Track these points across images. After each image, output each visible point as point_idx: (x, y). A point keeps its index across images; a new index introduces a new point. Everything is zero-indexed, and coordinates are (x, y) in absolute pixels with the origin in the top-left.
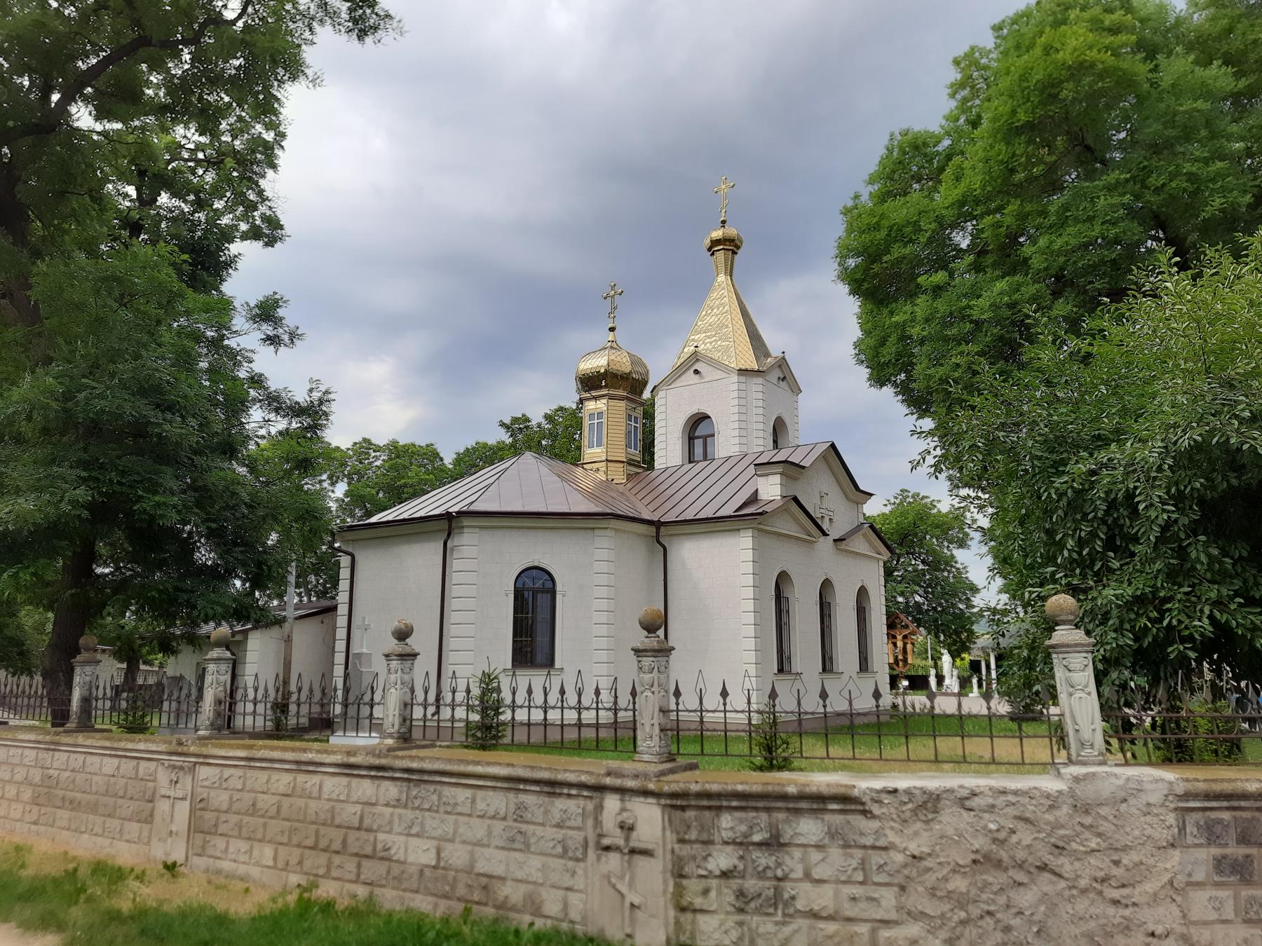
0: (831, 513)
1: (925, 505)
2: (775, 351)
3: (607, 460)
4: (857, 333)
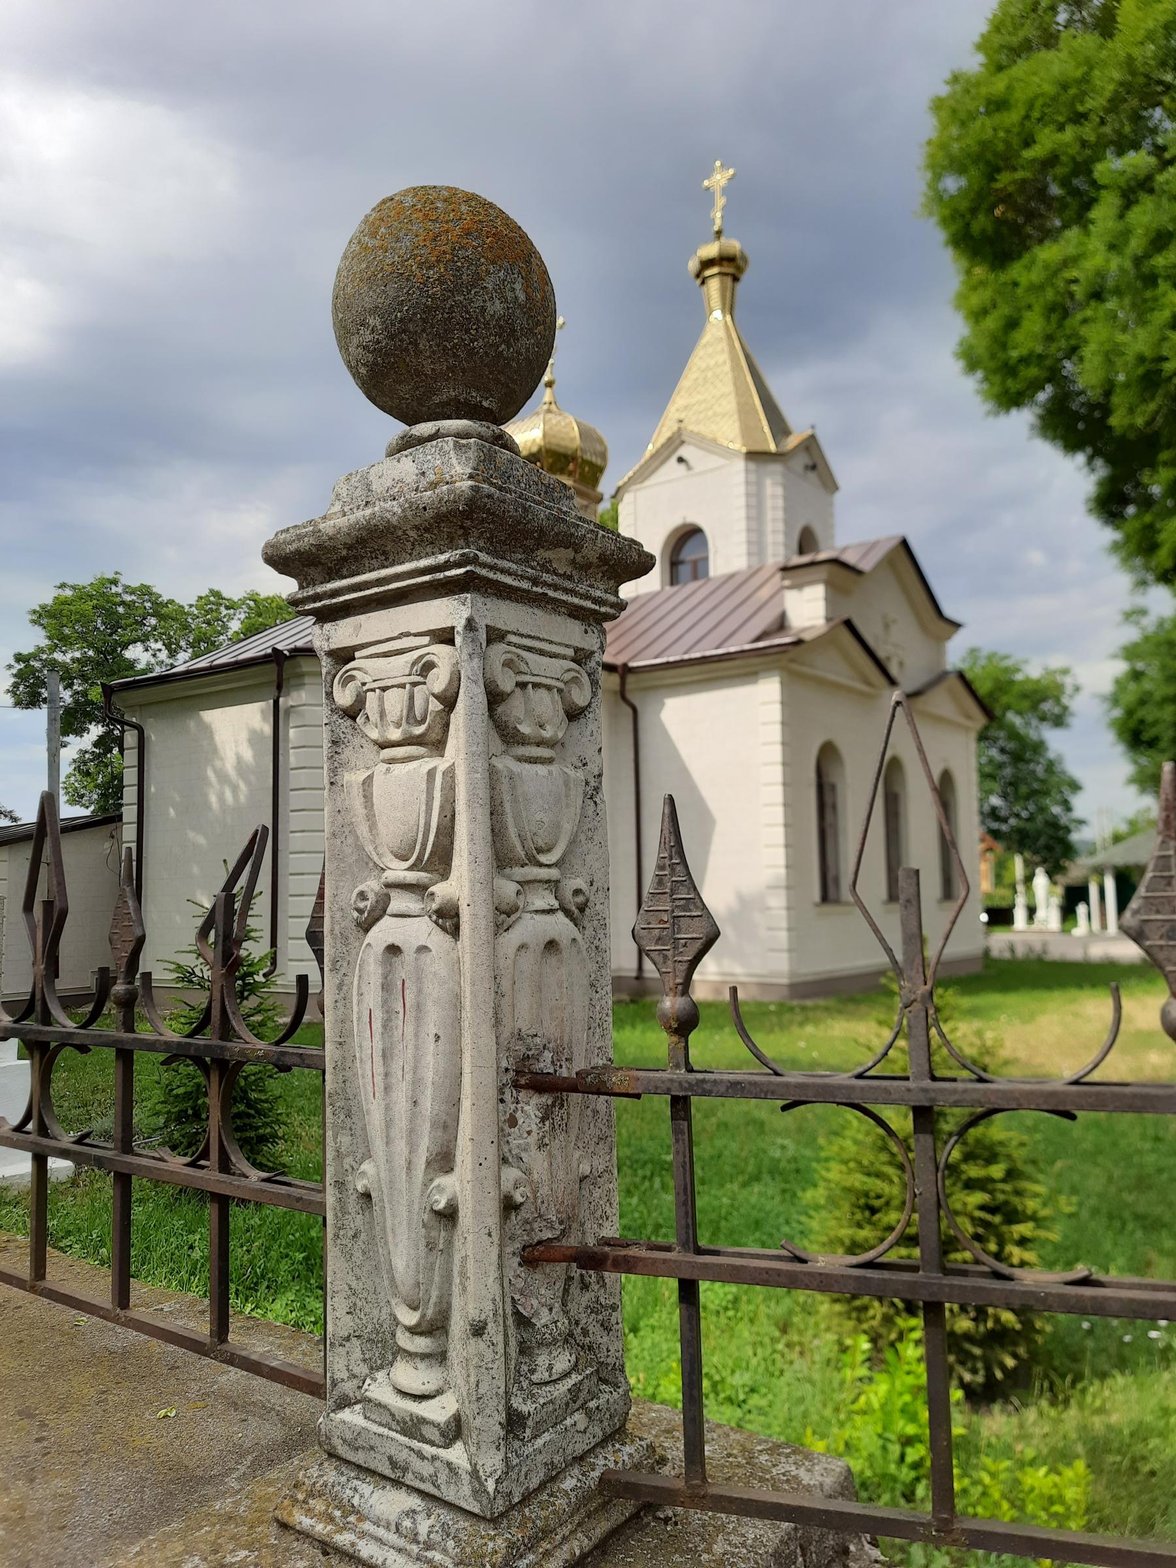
1: (1007, 670)
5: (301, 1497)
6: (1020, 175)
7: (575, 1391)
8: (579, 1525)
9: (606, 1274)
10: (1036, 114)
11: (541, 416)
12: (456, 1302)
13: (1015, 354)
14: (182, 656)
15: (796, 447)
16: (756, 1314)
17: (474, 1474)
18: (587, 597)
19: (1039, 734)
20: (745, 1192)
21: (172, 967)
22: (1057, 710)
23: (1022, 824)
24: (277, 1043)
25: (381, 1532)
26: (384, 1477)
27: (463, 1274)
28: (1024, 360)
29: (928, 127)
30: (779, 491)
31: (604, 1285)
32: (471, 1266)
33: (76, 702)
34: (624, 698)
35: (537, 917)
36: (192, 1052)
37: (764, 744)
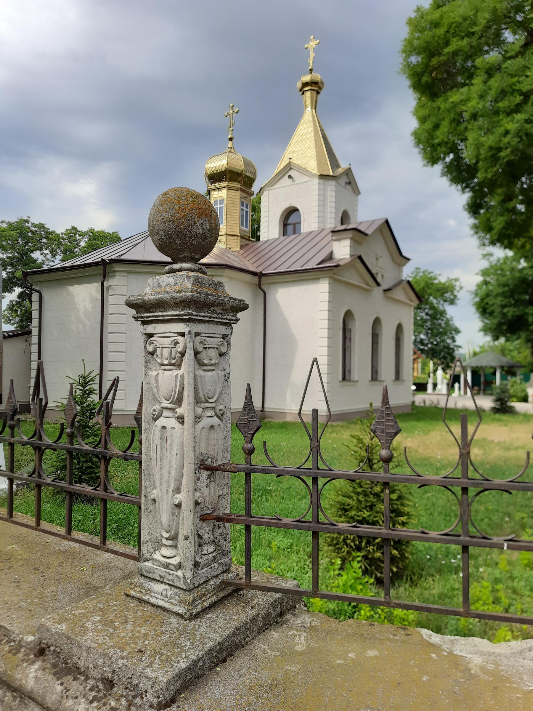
0: (383, 271)
1: (431, 278)
2: (344, 165)
3: (226, 234)
4: (413, 124)
5: (132, 587)
6: (442, 58)
7: (214, 558)
8: (214, 594)
9: (226, 524)
10: (452, 31)
11: (227, 154)
12: (180, 531)
13: (436, 141)
14: (59, 257)
15: (342, 174)
16: (299, 551)
17: (184, 578)
18: (227, 319)
19: (443, 307)
20: (299, 503)
21: (60, 404)
22: (452, 297)
23: (433, 347)
24: (124, 452)
25: (157, 595)
26: (158, 581)
27: (183, 523)
28: (439, 144)
29: (405, 32)
30: (334, 194)
31: (225, 527)
32: (185, 520)
33: (9, 277)
34: (260, 288)
35: (208, 419)
36: (95, 453)
37: (321, 311)
